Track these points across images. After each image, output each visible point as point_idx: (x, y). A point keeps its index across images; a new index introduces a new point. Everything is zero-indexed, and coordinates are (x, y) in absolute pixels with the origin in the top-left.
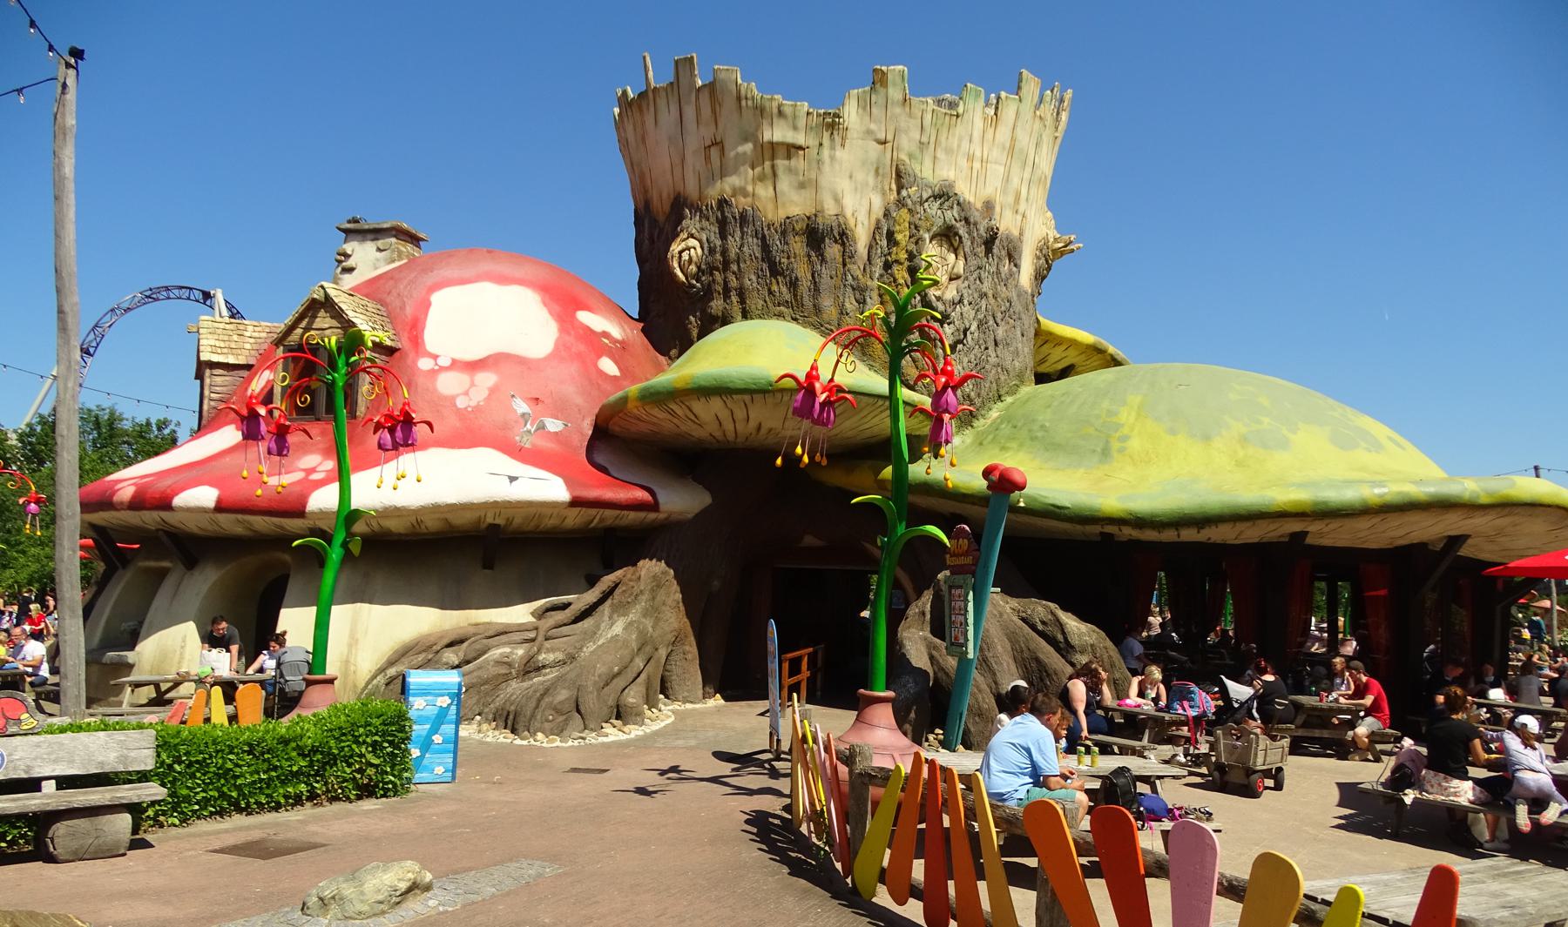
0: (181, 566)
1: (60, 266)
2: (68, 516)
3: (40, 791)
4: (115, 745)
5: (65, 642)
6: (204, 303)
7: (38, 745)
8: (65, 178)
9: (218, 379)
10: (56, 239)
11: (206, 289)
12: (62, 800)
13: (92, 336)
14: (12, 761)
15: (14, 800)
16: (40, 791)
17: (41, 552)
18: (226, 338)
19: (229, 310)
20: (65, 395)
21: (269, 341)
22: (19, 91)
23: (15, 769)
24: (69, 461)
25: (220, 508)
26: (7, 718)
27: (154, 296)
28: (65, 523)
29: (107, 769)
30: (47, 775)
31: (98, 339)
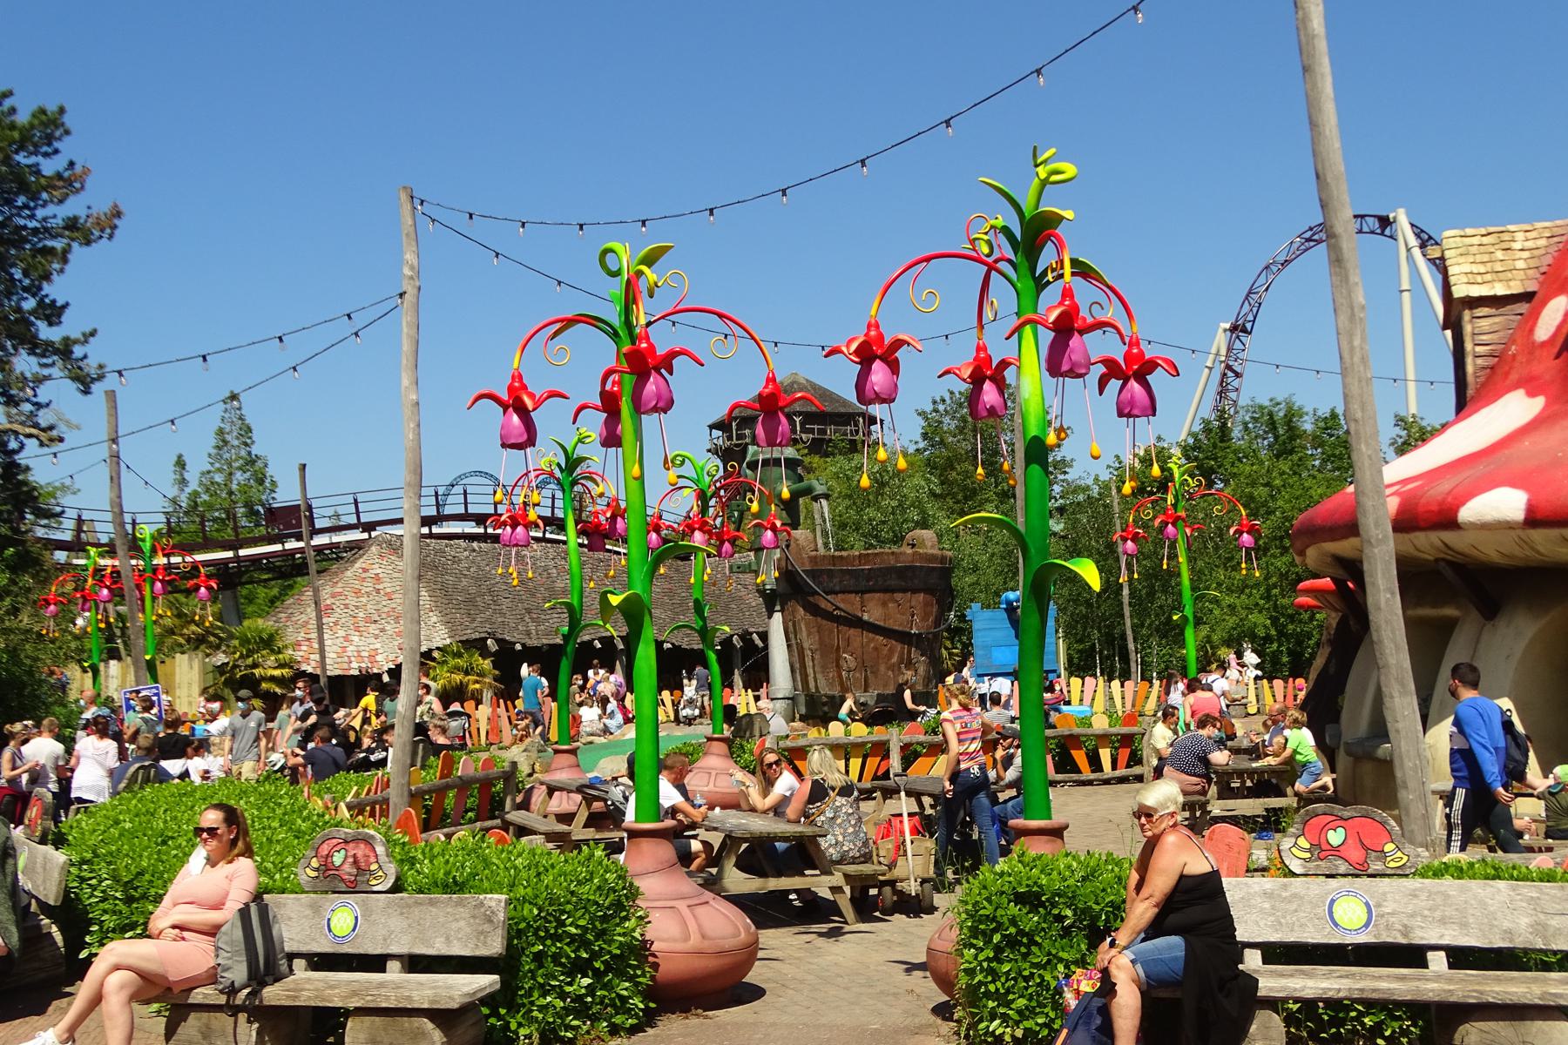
0: (1475, 615)
1: (1323, 168)
2: (1378, 540)
3: (1426, 967)
4: (1524, 905)
5: (1397, 731)
6: (1382, 234)
7: (1414, 895)
8: (1314, 37)
9: (1484, 323)
10: (1312, 130)
11: (1383, 213)
12: (1471, 988)
13: (1246, 307)
14: (1383, 916)
15: (1402, 978)
16: (1426, 967)
17: (1237, 601)
18: (1486, 258)
19: (1418, 236)
20: (1352, 358)
21: (1553, 249)
22: (1135, 9)
23: (1388, 927)
24: (1370, 457)
25: (1534, 519)
26: (1366, 849)
27: (1316, 237)
28: (1376, 551)
29: (1519, 943)
30: (1433, 942)
31: (1255, 310)
